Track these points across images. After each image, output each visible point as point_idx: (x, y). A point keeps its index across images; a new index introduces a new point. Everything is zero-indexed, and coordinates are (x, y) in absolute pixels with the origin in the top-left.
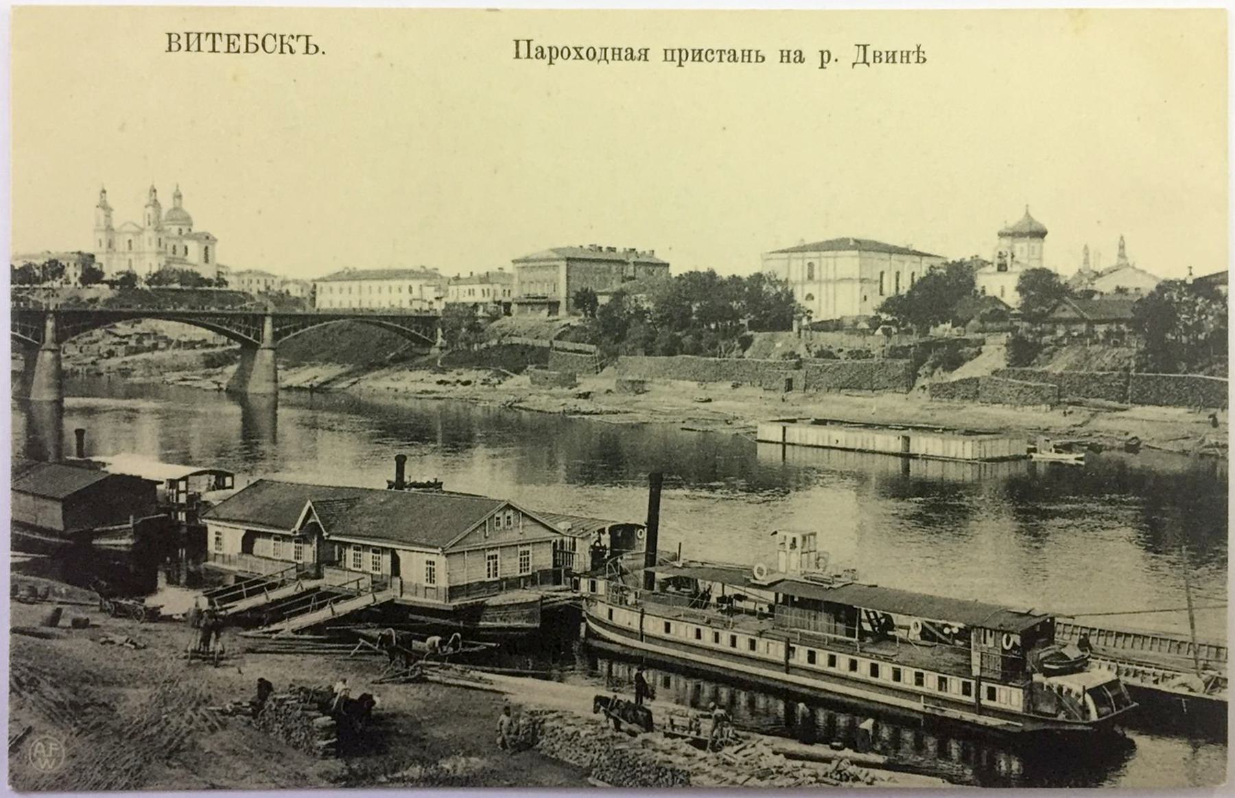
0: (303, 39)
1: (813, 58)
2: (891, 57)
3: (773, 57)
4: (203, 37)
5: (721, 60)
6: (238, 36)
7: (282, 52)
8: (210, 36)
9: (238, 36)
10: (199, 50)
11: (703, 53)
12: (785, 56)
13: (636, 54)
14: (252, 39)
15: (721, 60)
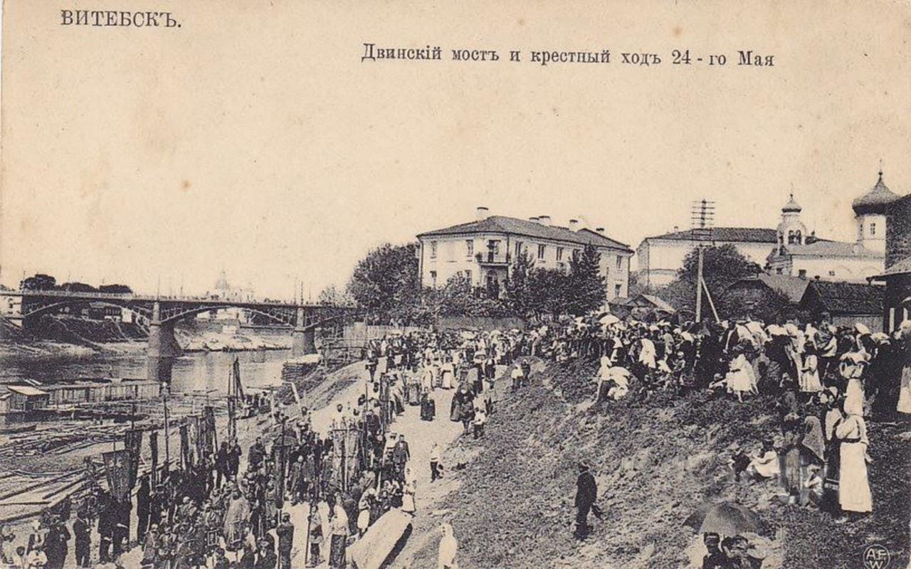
0: (165, 16)
1: (525, 56)
2: (391, 54)
3: (667, 59)
4: (89, 14)
5: (572, 60)
6: (115, 13)
7: (148, 24)
8: (95, 14)
9: (115, 13)
10: (86, 24)
11: (461, 53)
12: (722, 60)
13: (763, 61)
14: (125, 16)
15: (572, 60)
